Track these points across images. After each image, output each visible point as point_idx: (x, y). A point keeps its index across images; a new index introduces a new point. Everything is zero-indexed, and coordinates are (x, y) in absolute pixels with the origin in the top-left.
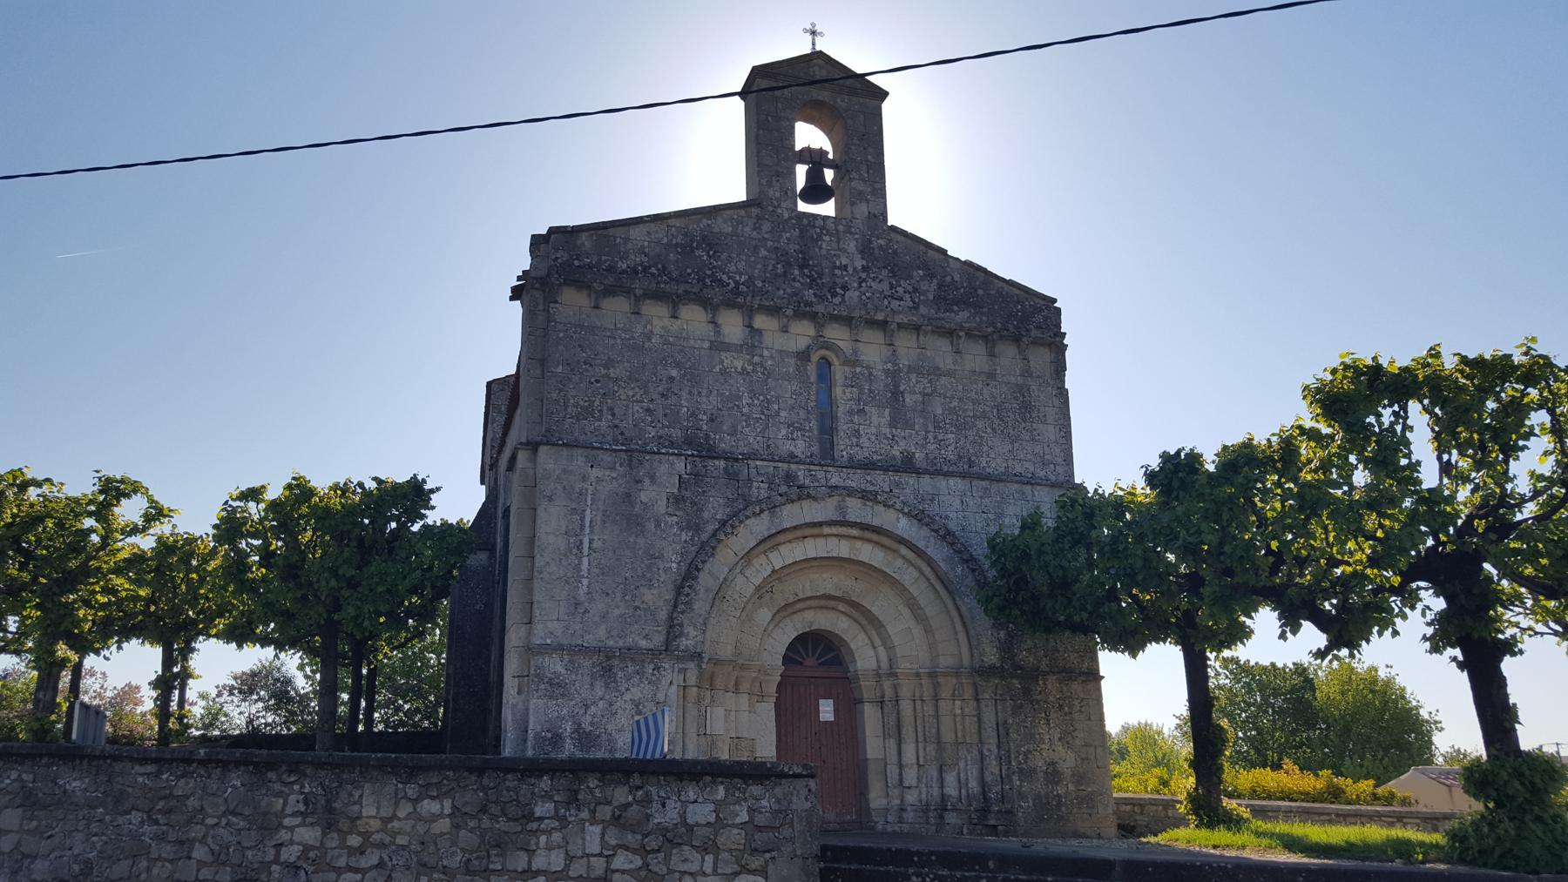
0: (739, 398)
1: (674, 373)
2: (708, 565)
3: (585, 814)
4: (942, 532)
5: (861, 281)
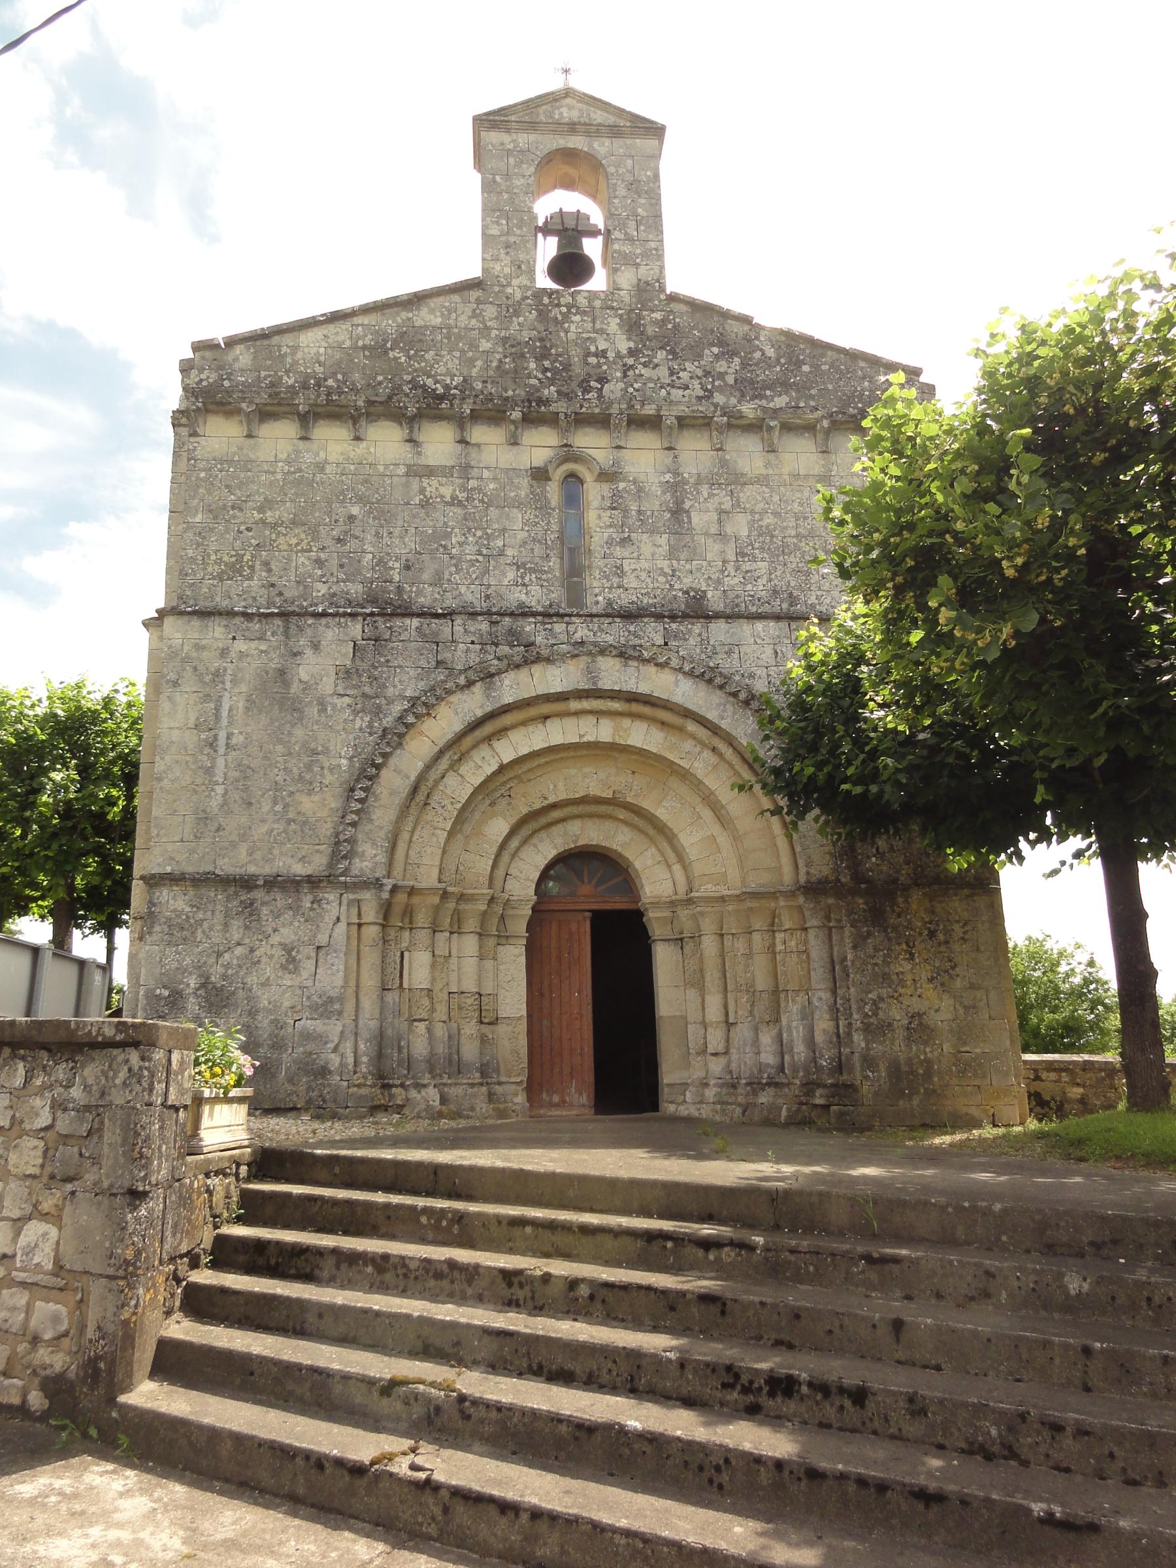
0: (448, 536)
1: (355, 510)
2: (393, 761)
4: (743, 696)
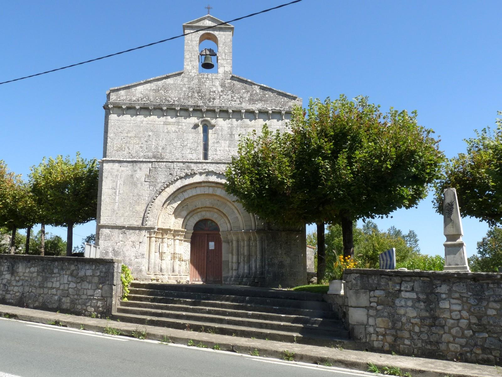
1: (150, 133)
3: (64, 272)
5: (220, 96)
